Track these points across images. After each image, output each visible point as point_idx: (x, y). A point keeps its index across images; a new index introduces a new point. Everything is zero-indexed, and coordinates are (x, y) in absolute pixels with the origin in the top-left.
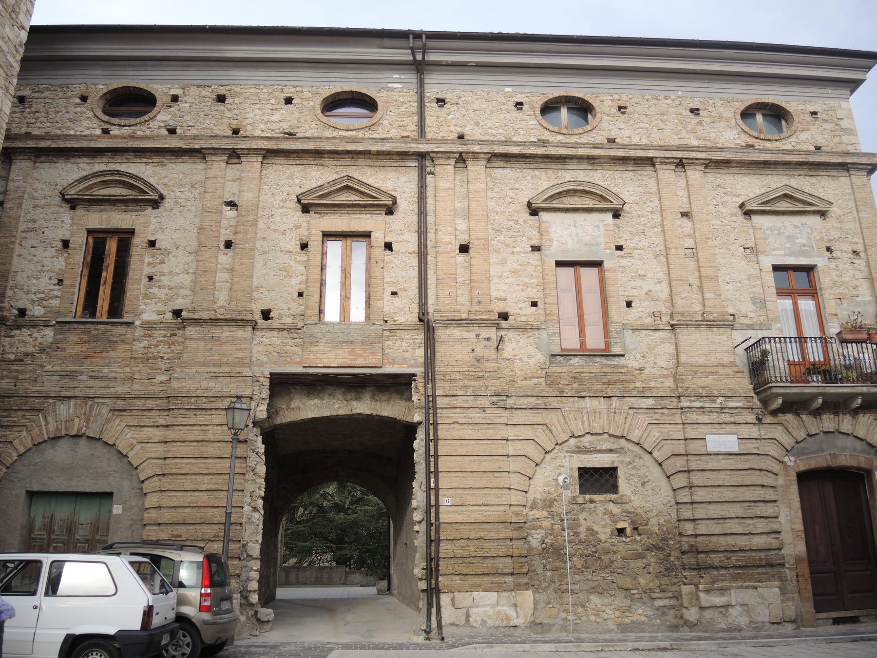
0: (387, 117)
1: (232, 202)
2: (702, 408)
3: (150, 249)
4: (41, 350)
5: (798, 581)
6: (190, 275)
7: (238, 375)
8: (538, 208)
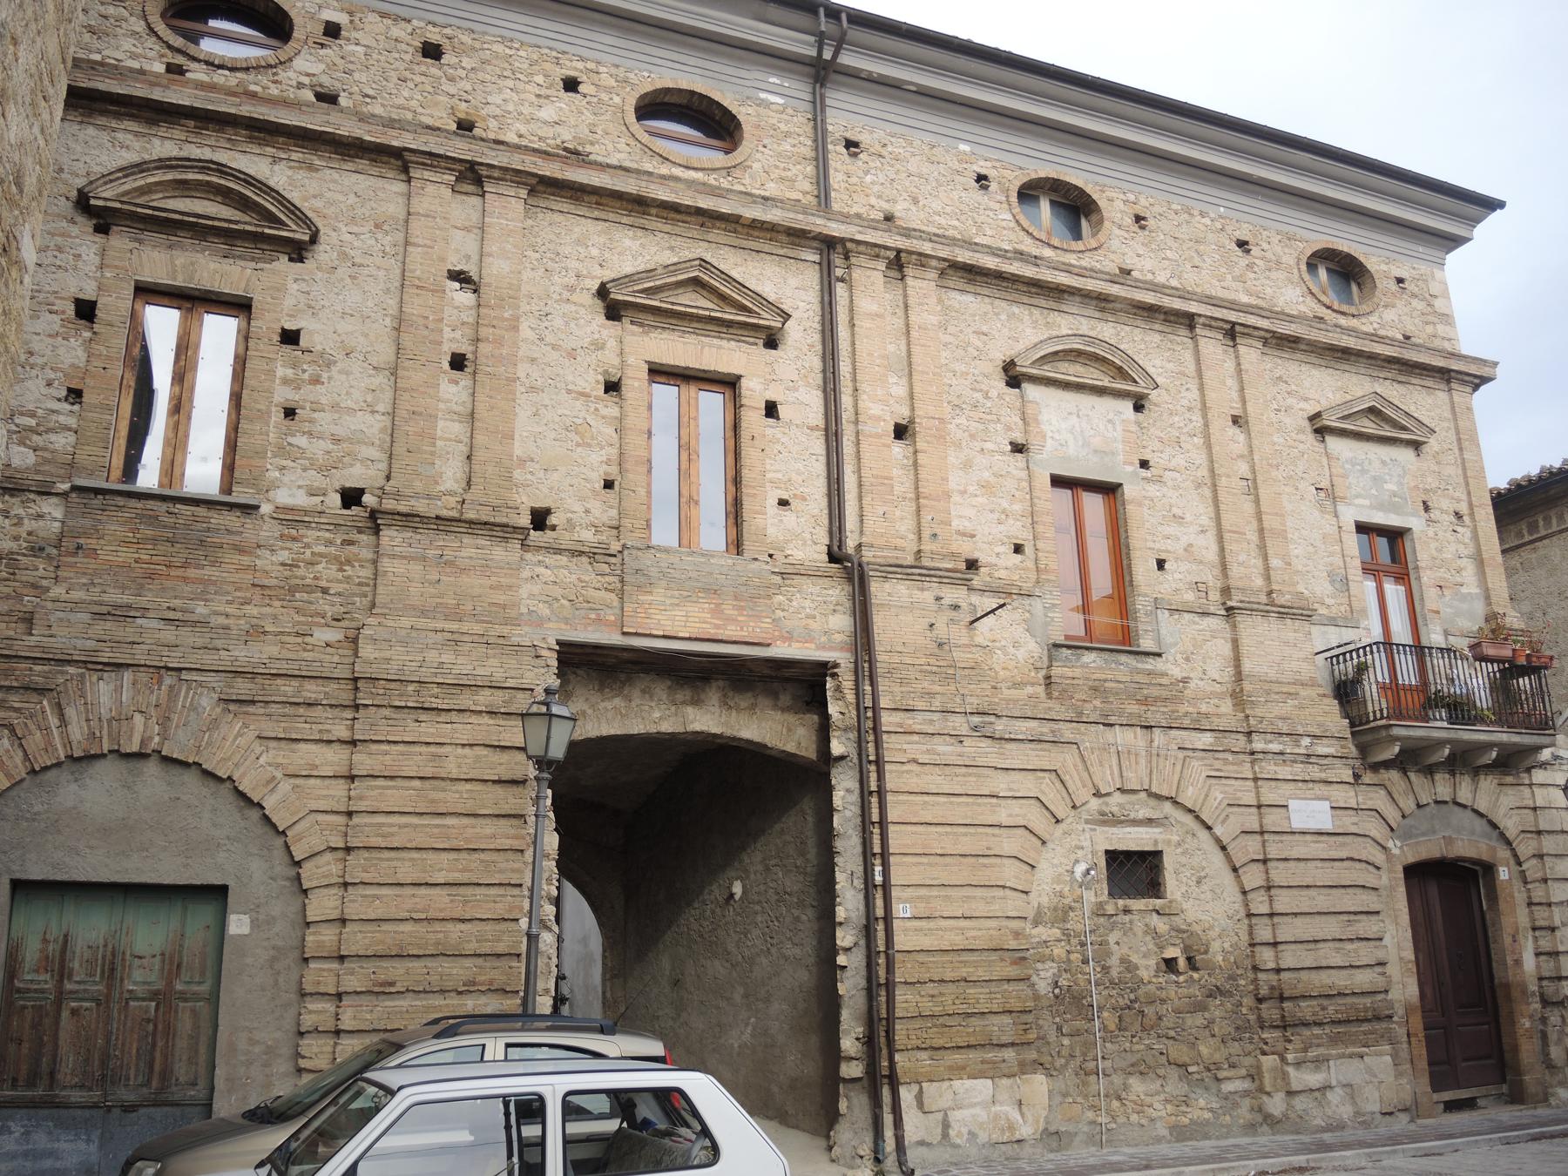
0: (758, 156)
1: (461, 272)
2: (1282, 753)
3: (287, 349)
4: (32, 549)
5: (1409, 1043)
6: (378, 417)
7: (501, 641)
8: (1024, 375)
